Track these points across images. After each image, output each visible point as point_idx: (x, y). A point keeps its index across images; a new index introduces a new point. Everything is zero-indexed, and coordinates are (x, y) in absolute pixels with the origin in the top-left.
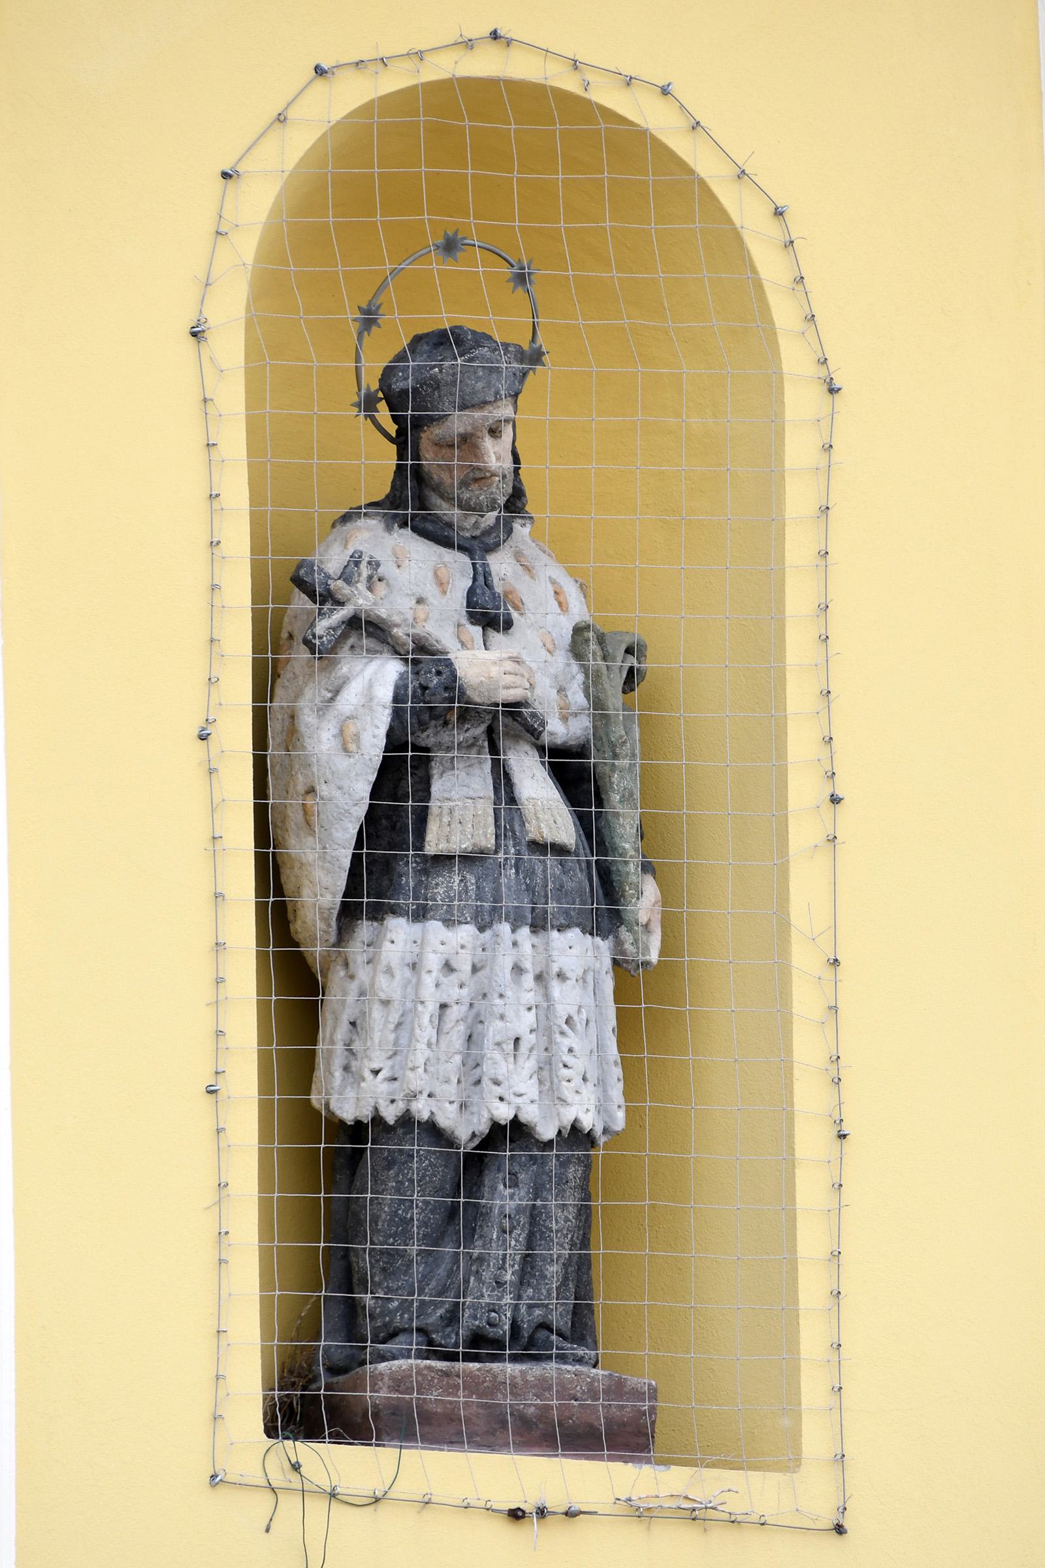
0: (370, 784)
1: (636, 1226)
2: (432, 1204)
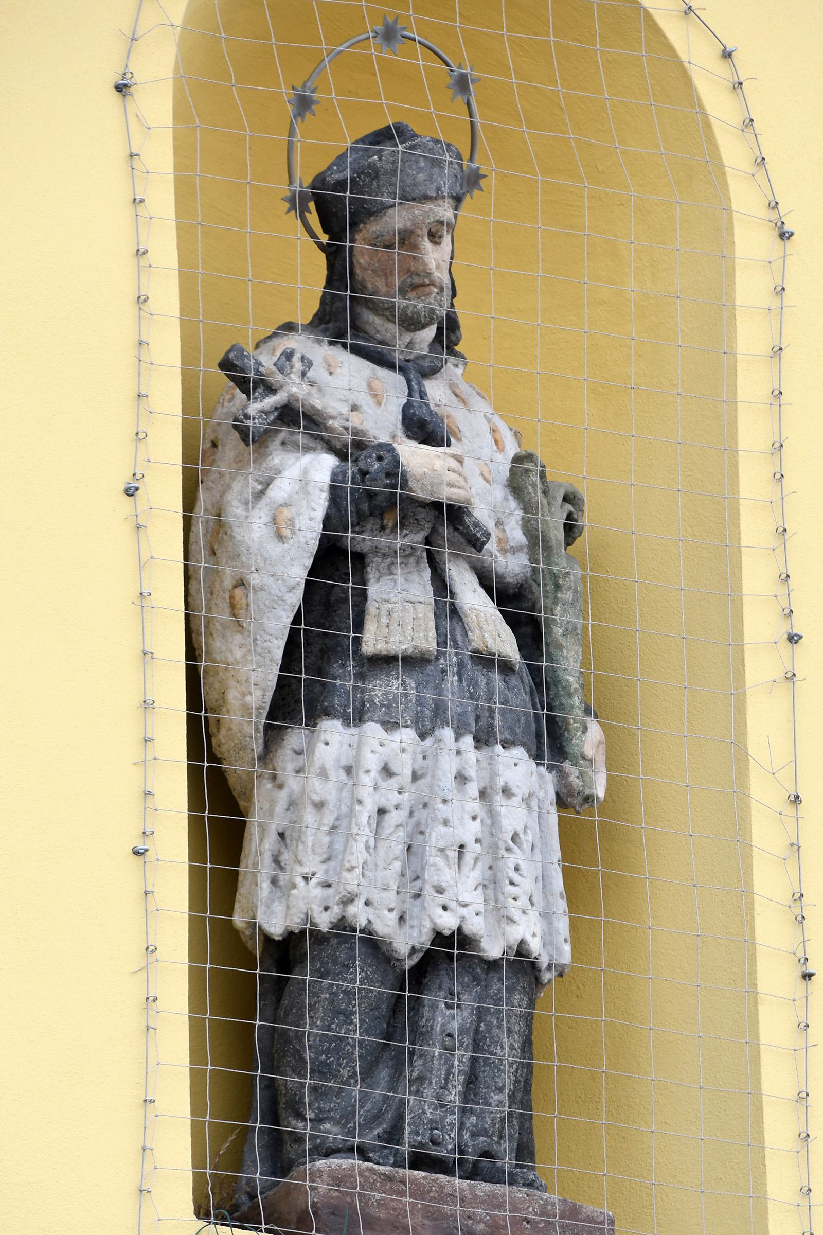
1: (574, 1099)
2: (367, 1023)
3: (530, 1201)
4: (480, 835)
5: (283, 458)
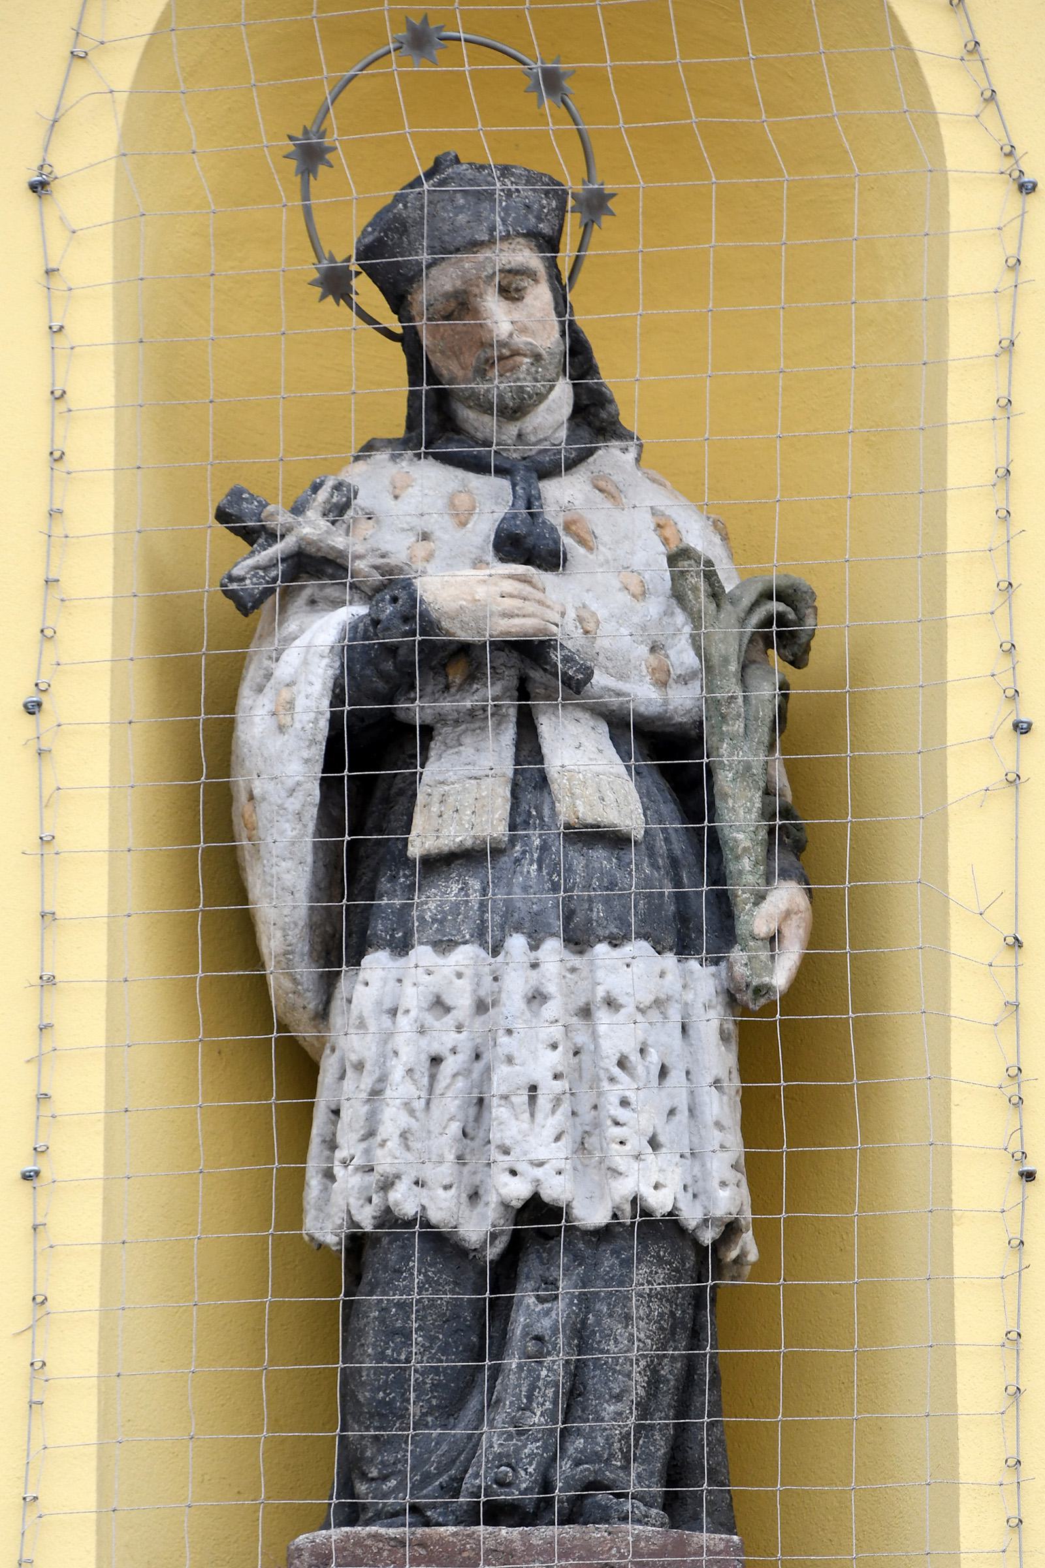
3: (613, 1541)
4: (560, 1069)
5: (302, 622)
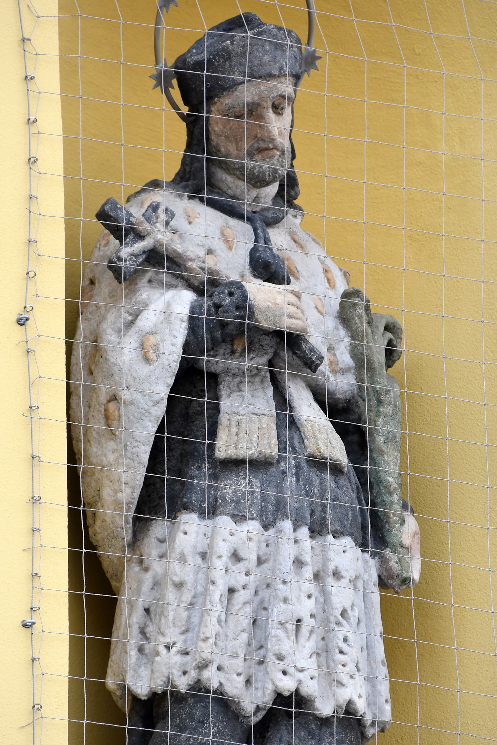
0: (168, 387)
4: (314, 611)
